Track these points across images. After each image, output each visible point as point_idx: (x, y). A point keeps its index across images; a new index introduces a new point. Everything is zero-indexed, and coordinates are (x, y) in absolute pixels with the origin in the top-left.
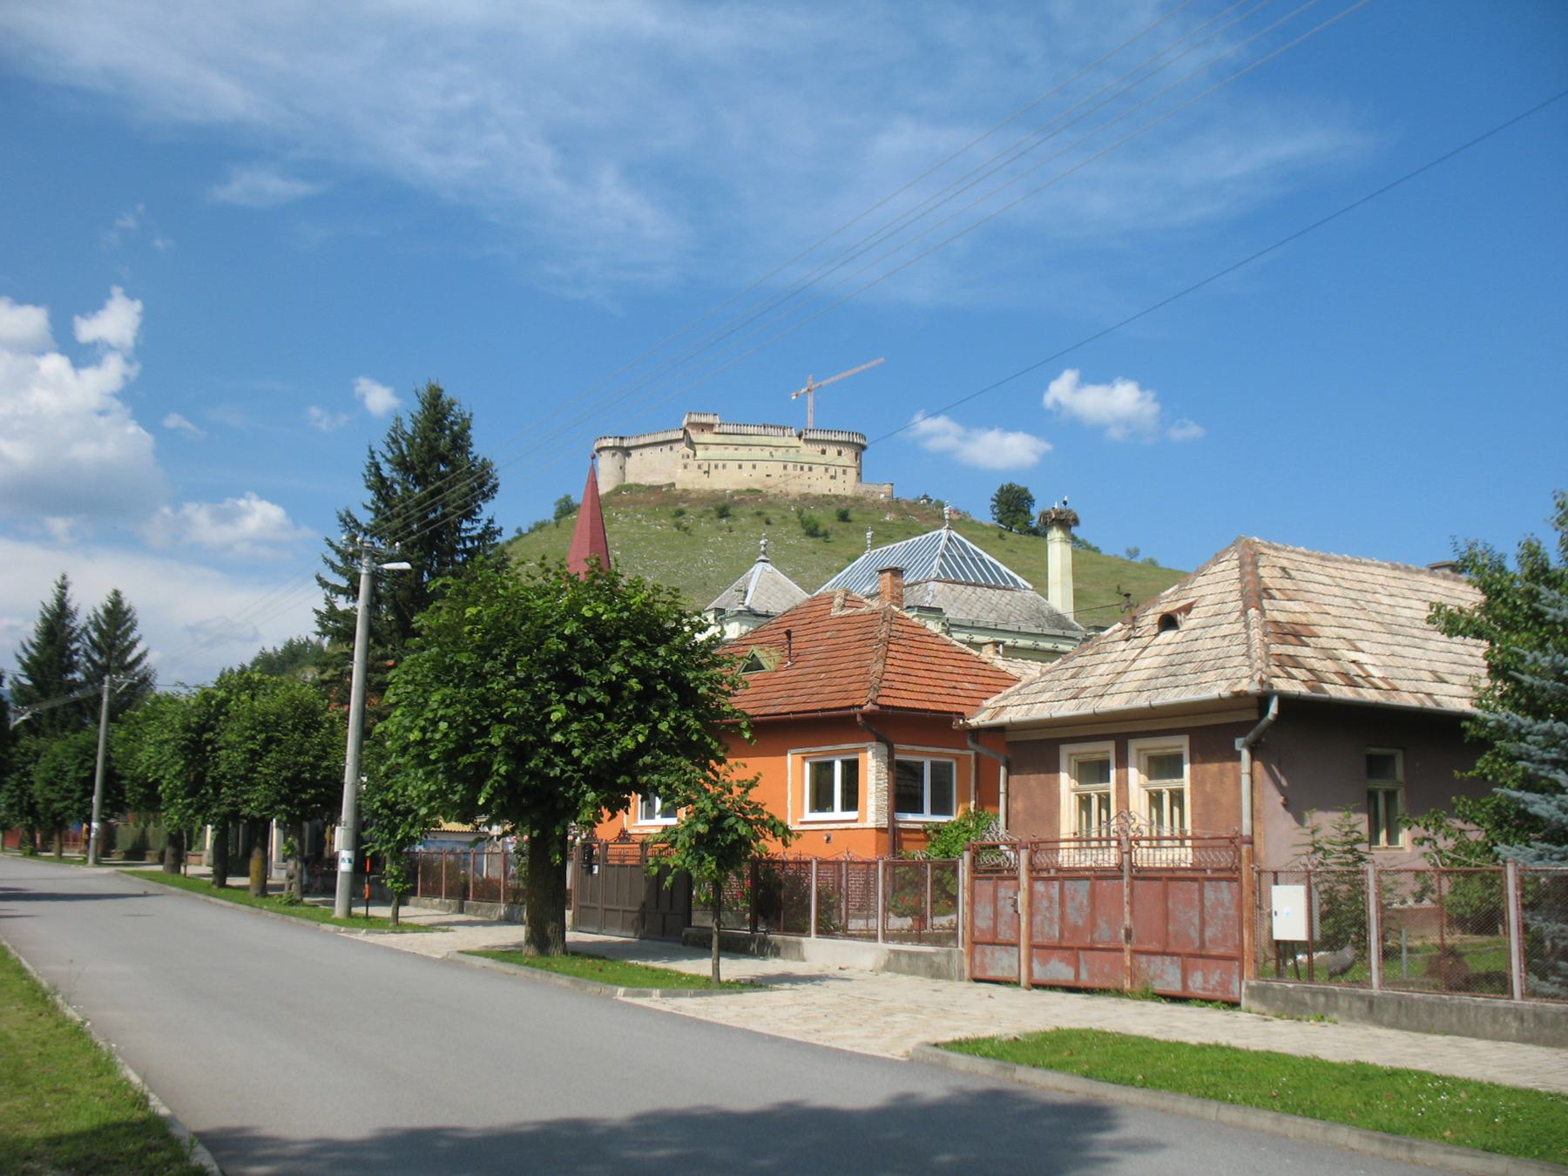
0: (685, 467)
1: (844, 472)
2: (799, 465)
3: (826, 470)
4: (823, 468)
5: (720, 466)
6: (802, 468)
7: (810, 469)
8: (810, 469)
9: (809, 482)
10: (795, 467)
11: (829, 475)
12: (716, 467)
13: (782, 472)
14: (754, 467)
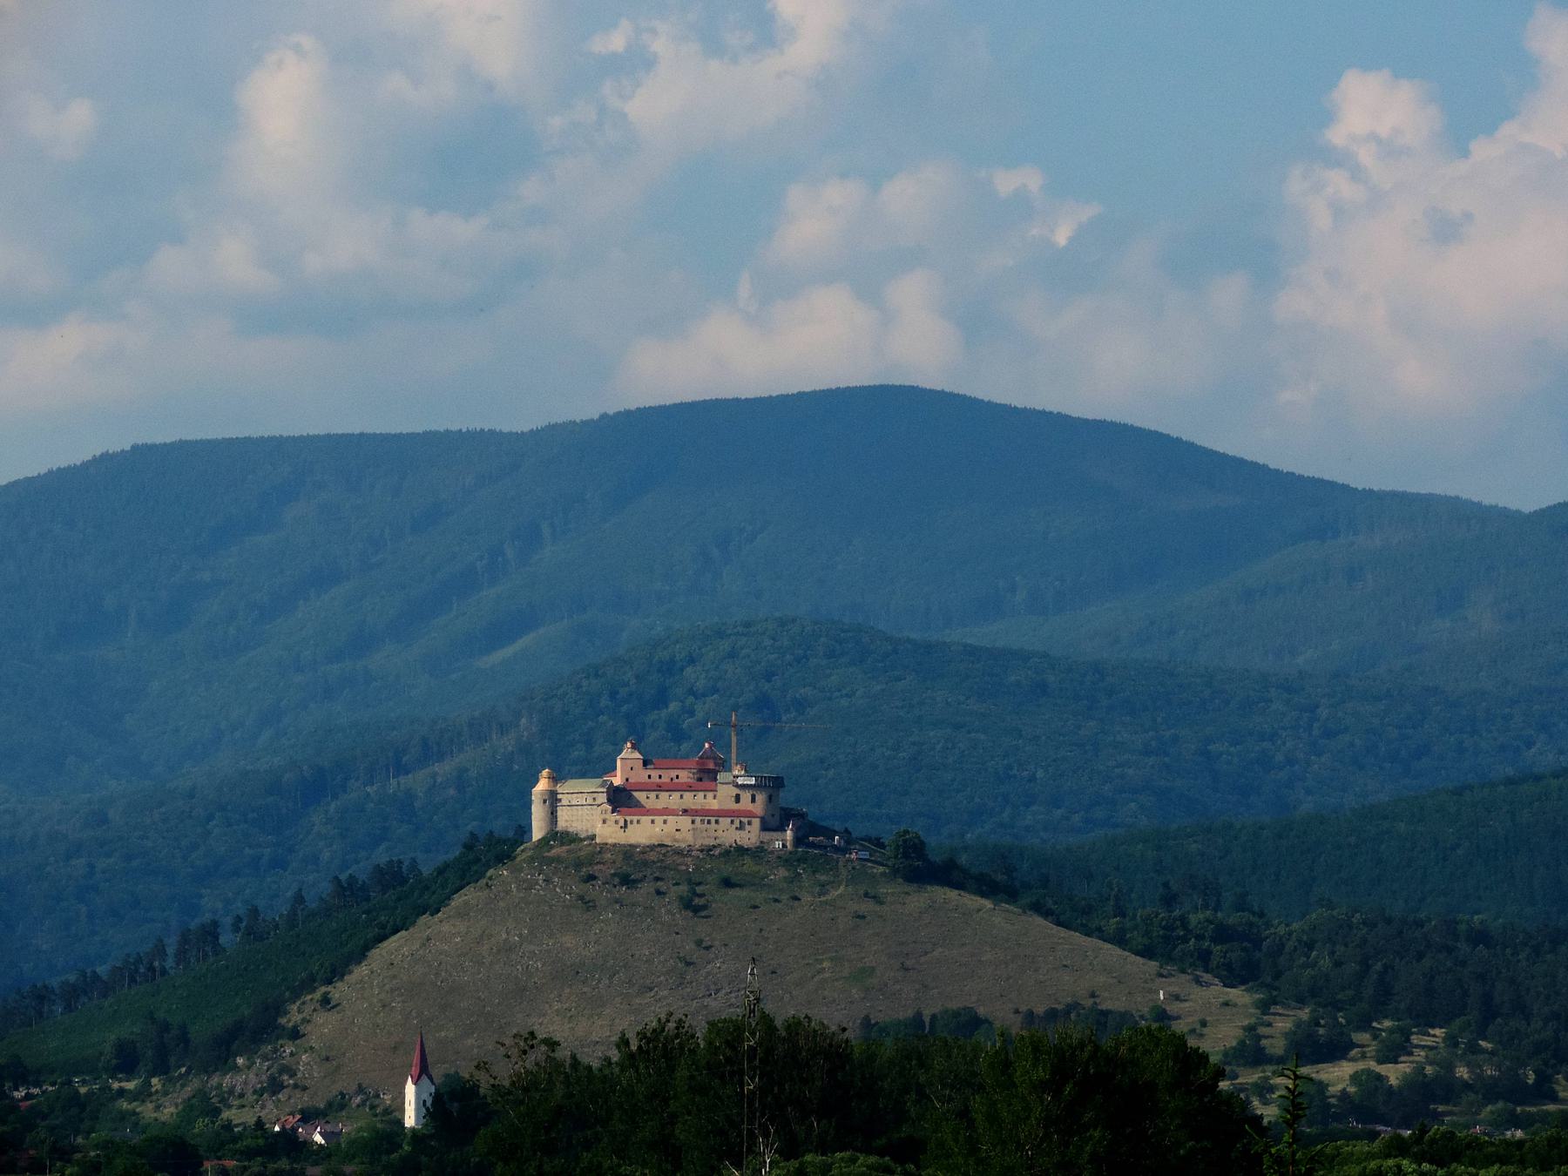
0: (604, 822)
1: (749, 823)
2: (713, 819)
3: (732, 822)
6: (709, 822)
7: (717, 822)
8: (717, 822)
11: (734, 826)
12: (631, 822)
13: (690, 826)
14: (665, 822)
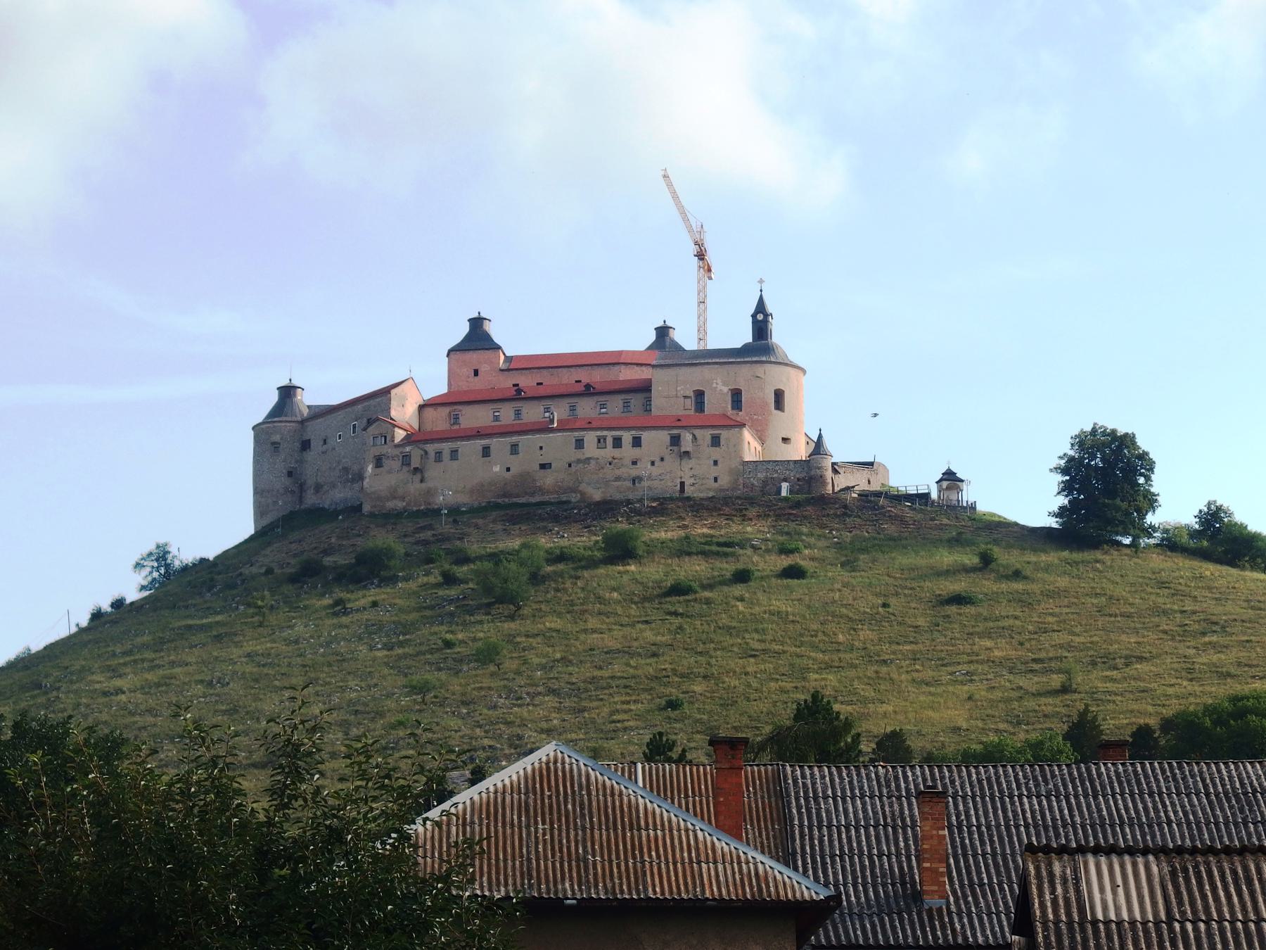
4: (664, 436)
5: (446, 455)
6: (617, 443)
8: (637, 442)
9: (634, 472)
10: (601, 441)
12: (439, 454)
